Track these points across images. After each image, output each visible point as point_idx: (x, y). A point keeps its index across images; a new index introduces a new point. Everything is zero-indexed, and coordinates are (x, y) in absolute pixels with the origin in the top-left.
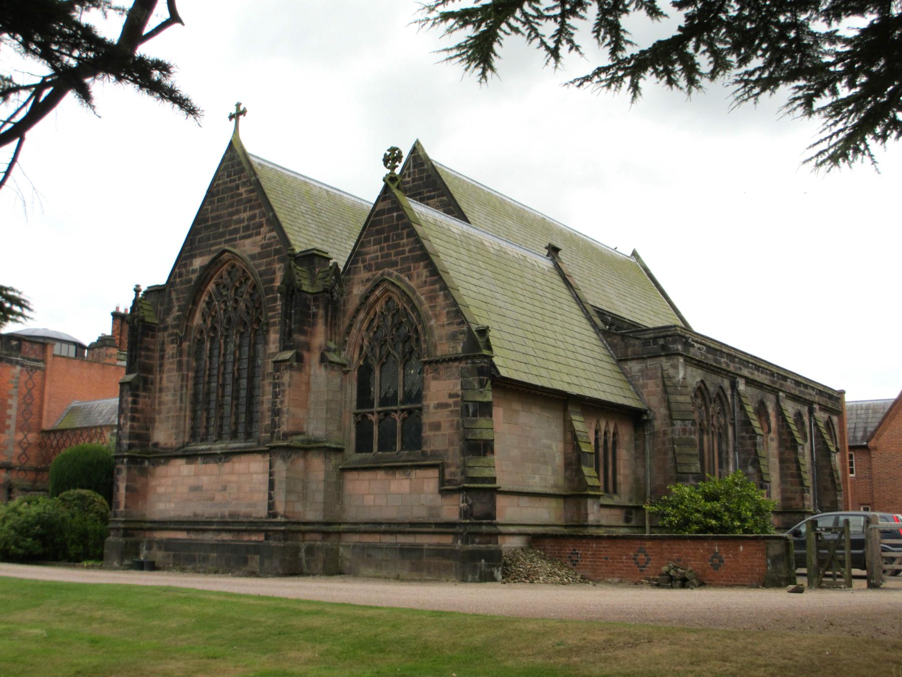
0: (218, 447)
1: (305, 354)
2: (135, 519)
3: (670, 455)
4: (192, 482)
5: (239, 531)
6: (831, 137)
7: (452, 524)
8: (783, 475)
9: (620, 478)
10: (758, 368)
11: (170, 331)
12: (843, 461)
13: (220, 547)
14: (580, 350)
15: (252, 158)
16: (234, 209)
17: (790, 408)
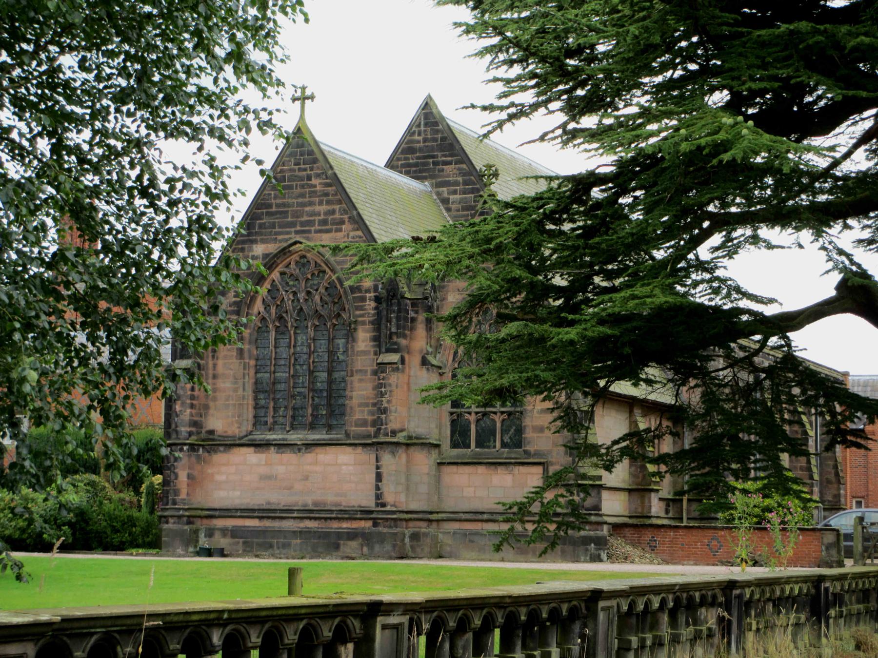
0: (295, 437)
1: (407, 357)
2: (194, 506)
4: (263, 470)
5: (326, 519)
13: (303, 534)
15: (322, 146)
16: (307, 200)
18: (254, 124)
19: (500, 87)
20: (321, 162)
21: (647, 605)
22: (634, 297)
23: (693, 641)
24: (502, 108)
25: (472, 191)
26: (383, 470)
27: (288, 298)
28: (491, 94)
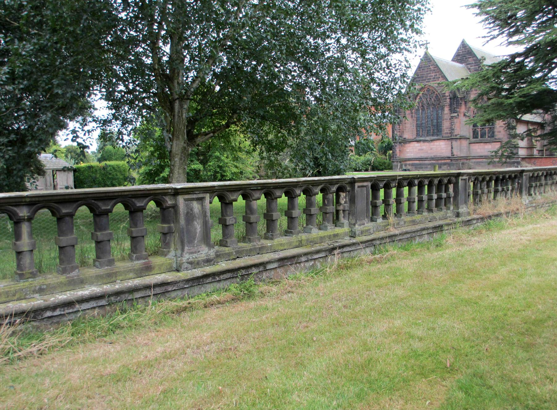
0: (428, 138)
18: (418, 46)
19: (488, 30)
20: (433, 62)
21: (538, 174)
22: (531, 88)
23: (551, 185)
24: (488, 37)
25: (477, 65)
26: (453, 146)
27: (424, 100)
28: (485, 32)
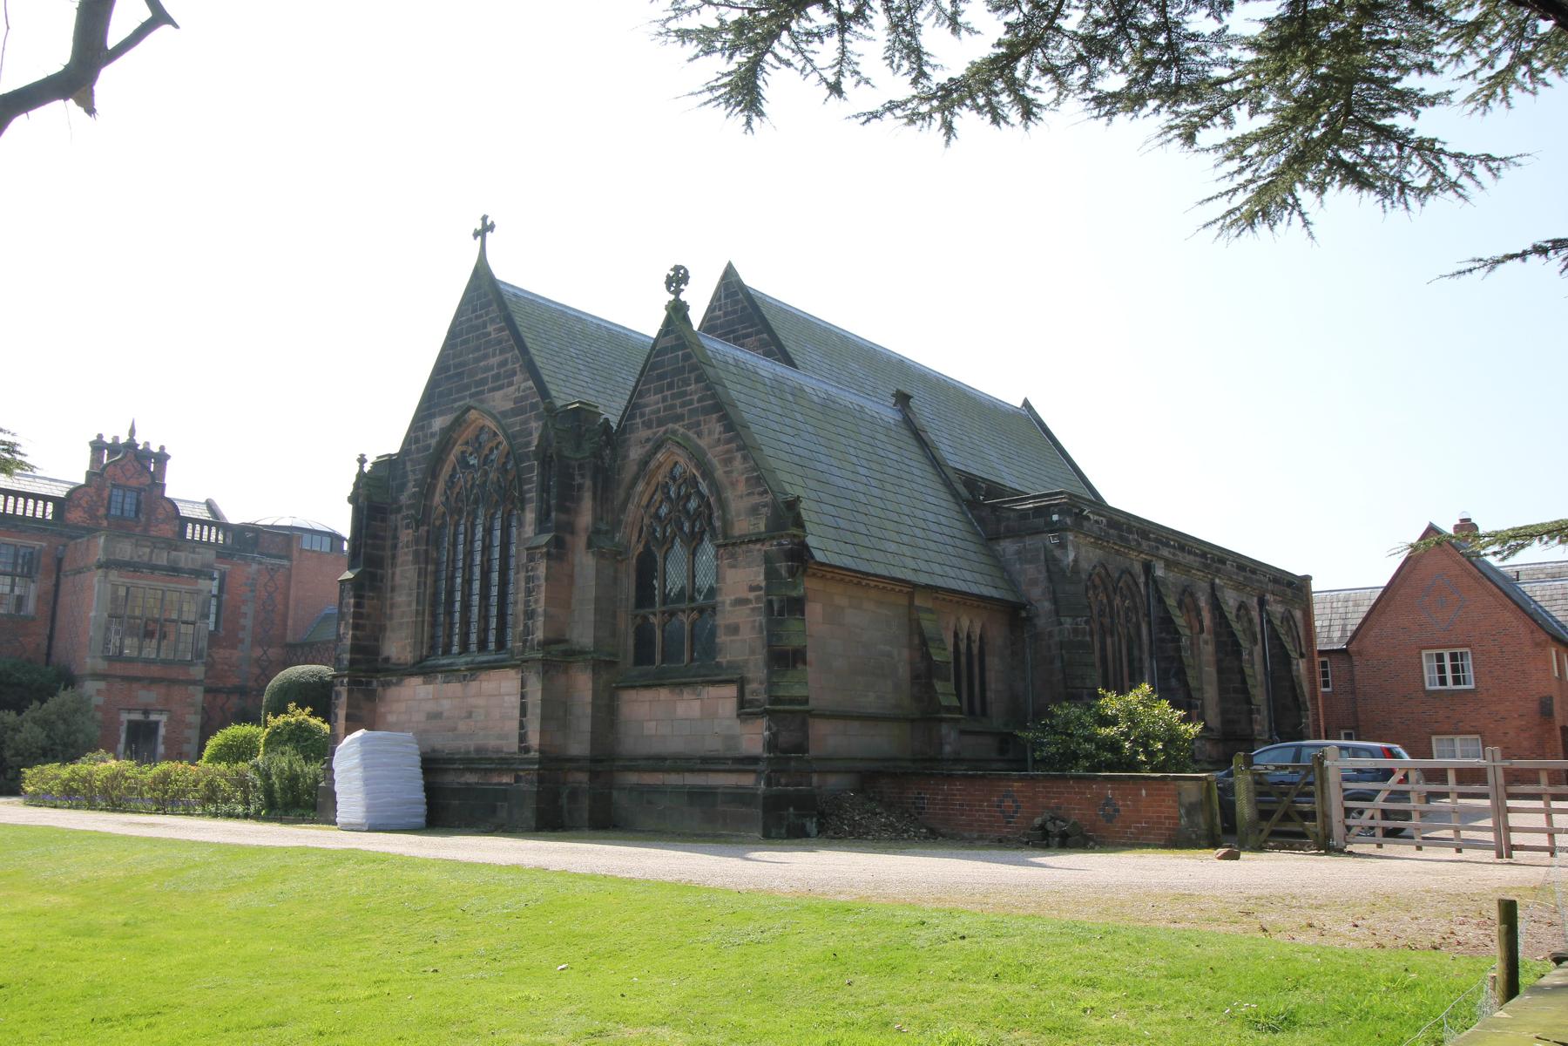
1: (568, 538)
3: (1058, 664)
4: (430, 706)
6: (1235, 191)
7: (754, 760)
8: (1222, 690)
9: (990, 695)
10: (1182, 548)
11: (405, 512)
12: (1311, 670)
14: (934, 527)
17: (1230, 599)
